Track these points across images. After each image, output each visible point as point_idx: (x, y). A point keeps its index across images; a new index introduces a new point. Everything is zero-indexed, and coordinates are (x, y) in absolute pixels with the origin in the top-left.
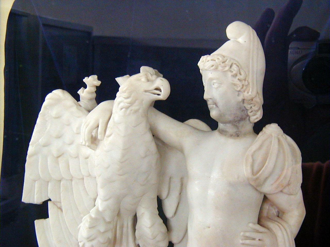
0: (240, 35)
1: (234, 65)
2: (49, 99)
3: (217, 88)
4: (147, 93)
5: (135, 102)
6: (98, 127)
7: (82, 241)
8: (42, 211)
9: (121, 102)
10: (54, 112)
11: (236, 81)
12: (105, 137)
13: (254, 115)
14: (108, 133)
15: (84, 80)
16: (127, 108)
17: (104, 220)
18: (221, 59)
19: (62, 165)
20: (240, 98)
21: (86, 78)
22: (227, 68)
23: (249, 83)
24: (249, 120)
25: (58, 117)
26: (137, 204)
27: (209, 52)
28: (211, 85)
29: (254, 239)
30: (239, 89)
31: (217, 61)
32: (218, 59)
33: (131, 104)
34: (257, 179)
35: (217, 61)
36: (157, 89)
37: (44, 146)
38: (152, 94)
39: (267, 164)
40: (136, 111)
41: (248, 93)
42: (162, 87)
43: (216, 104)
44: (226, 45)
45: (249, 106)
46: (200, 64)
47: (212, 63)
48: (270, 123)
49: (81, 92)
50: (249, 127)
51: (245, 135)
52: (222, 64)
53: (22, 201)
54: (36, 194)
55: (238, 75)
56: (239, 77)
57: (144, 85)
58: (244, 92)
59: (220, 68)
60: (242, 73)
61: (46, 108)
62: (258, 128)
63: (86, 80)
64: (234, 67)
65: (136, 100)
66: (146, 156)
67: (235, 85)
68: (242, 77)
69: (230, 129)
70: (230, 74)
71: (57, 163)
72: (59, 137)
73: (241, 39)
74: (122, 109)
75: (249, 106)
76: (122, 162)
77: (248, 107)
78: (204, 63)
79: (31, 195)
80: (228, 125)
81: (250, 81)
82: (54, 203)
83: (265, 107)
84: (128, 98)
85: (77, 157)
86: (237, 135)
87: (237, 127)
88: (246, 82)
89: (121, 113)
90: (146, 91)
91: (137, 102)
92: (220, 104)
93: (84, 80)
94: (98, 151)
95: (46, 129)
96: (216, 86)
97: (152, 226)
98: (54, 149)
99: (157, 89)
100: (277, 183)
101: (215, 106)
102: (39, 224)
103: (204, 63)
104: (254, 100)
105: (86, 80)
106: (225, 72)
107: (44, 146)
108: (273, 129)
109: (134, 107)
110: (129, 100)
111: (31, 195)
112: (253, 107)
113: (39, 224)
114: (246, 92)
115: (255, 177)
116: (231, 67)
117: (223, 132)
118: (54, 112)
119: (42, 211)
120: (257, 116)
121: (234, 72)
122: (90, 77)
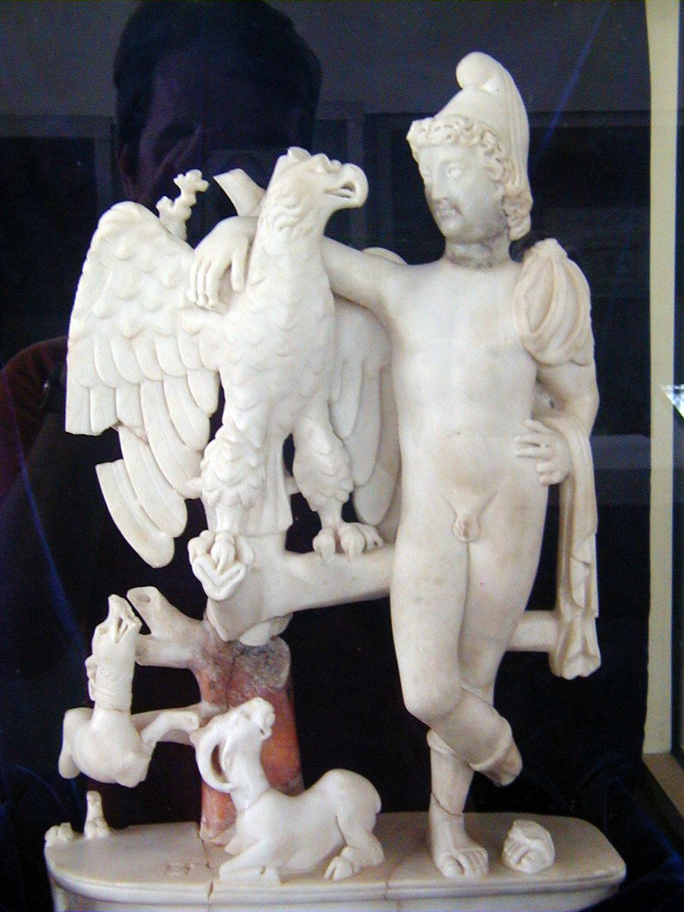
0: (486, 77)
1: (474, 134)
2: (108, 222)
3: (457, 180)
4: (330, 196)
5: (308, 211)
6: (230, 267)
7: (218, 488)
8: (107, 446)
9: (281, 214)
10: (120, 249)
11: (492, 162)
12: (248, 286)
13: (517, 226)
14: (254, 276)
15: (176, 181)
16: (292, 226)
17: (251, 444)
18: (462, 123)
19: (141, 352)
20: (499, 193)
21: (180, 176)
22: (476, 140)
23: (513, 167)
24: (508, 235)
25: (127, 259)
26: (299, 414)
27: (430, 112)
28: (444, 174)
29: (537, 445)
30: (497, 177)
31: (456, 127)
32: (458, 123)
33: (301, 217)
34: (540, 337)
35: (456, 127)
36: (345, 187)
37: (104, 317)
38: (336, 197)
39: (552, 309)
40: (309, 231)
41: (513, 183)
42: (348, 184)
43: (456, 208)
44: (458, 99)
45: (512, 209)
46: (411, 136)
47: (443, 133)
48: (542, 238)
49: (163, 203)
50: (503, 249)
51: (501, 263)
52: (465, 132)
53: (67, 430)
54: (94, 415)
55: (496, 150)
56: (498, 155)
57: (312, 182)
58: (507, 181)
59: (463, 140)
60: (502, 147)
61: (103, 240)
62: (519, 250)
63: (179, 181)
64: (488, 136)
65: (310, 208)
66: (325, 316)
67: (491, 170)
68: (502, 155)
69: (475, 252)
70: (481, 151)
71: (131, 350)
72: (130, 298)
73: (483, 85)
74: (281, 228)
75: (512, 209)
76: (288, 331)
77: (509, 209)
78: (420, 134)
79: (83, 417)
80: (474, 246)
81: (515, 161)
82: (130, 429)
83: (535, 214)
84: (294, 206)
85: (173, 334)
86: (490, 265)
87: (490, 249)
88: (510, 163)
89: (281, 236)
90: (327, 192)
91: (311, 215)
92: (466, 208)
93: (176, 181)
94: (234, 315)
95: (104, 283)
96: (455, 174)
97: (332, 451)
98: (124, 322)
99: (345, 187)
100: (570, 343)
101: (453, 212)
102: (106, 473)
103: (420, 134)
104: (522, 196)
105: (179, 181)
106: (471, 148)
107: (104, 317)
108: (550, 249)
109: (306, 224)
110: (297, 210)
111: (83, 417)
112: (519, 211)
113: (106, 473)
114: (510, 182)
115: (536, 335)
116: (482, 137)
117: (459, 261)
118: (120, 249)
119: (107, 446)
120: (521, 228)
121: (490, 147)
122: (189, 174)
